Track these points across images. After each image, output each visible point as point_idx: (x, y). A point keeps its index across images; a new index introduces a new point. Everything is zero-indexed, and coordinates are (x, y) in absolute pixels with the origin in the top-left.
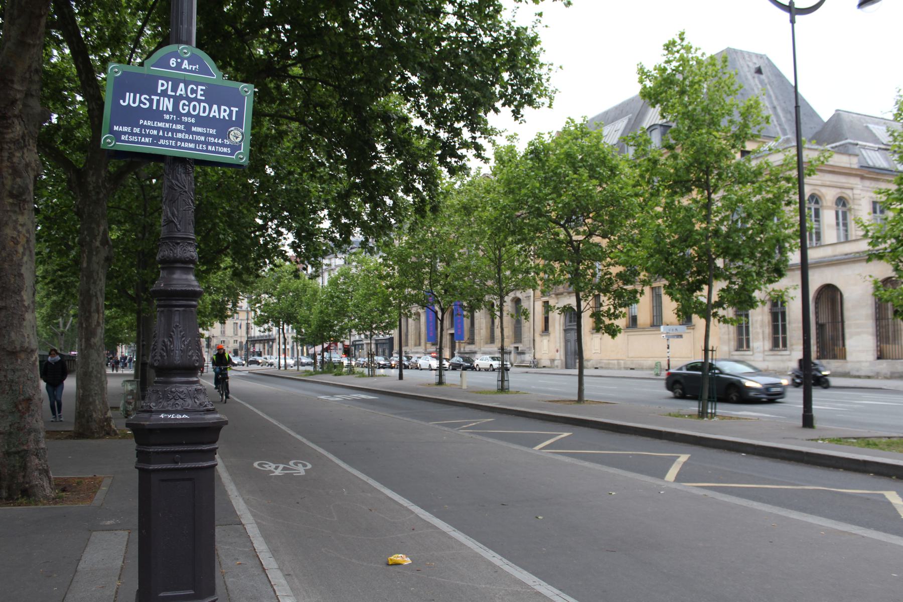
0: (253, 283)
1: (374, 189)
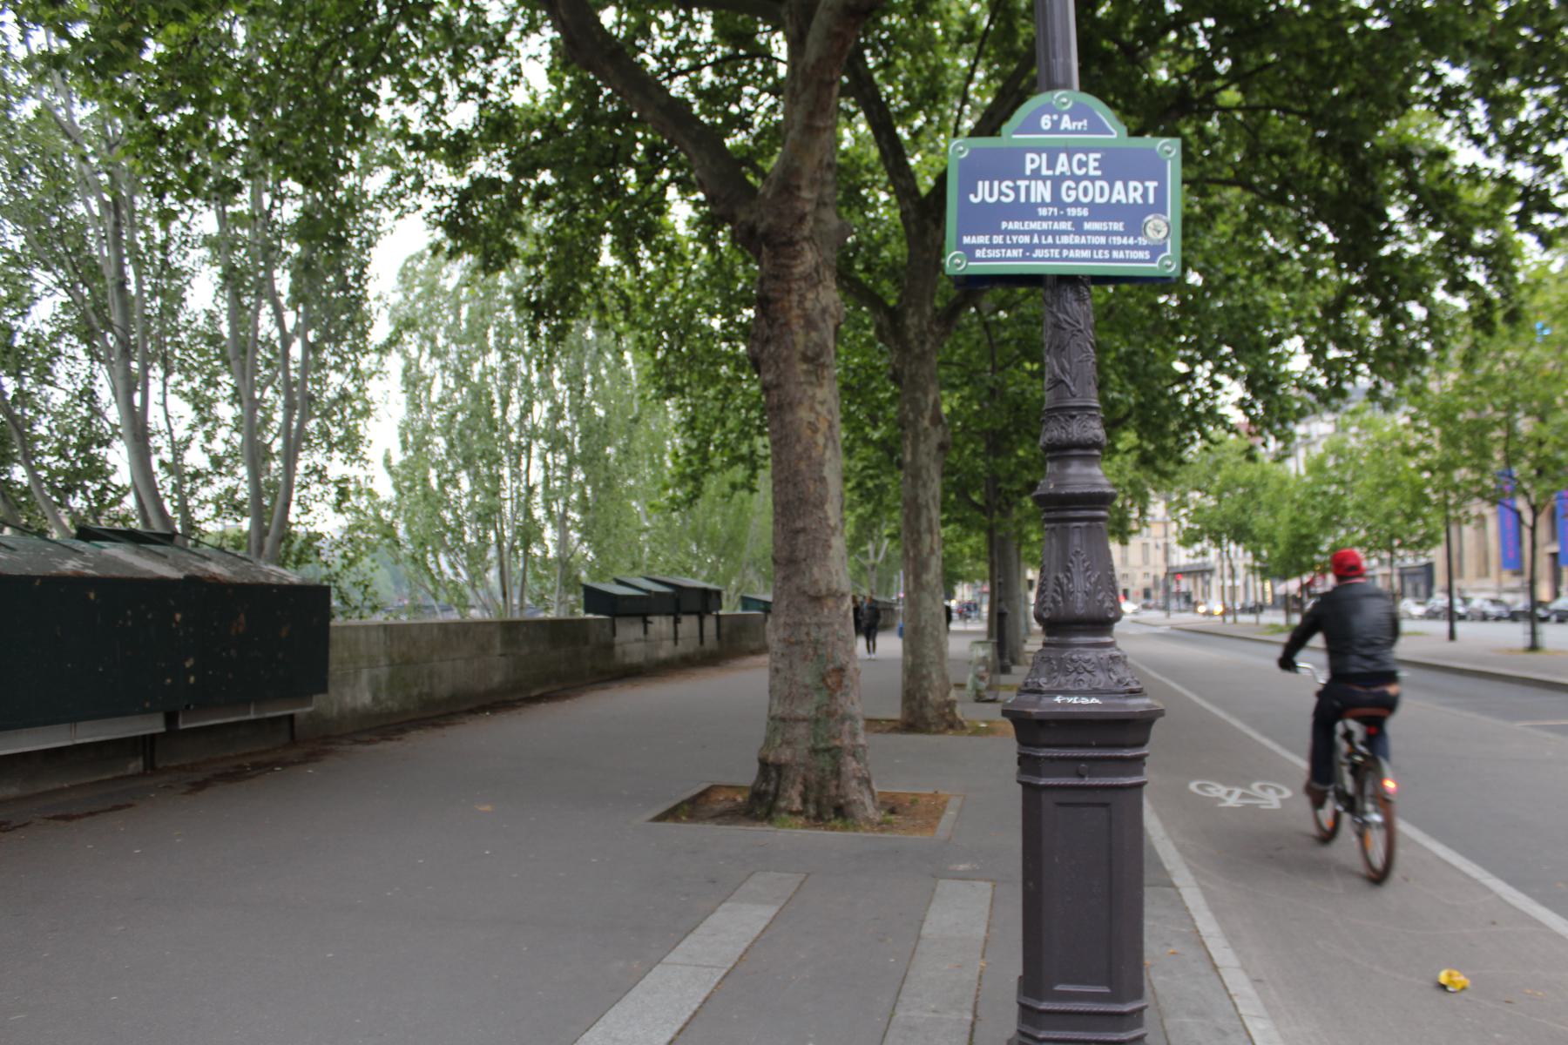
0: (1174, 473)
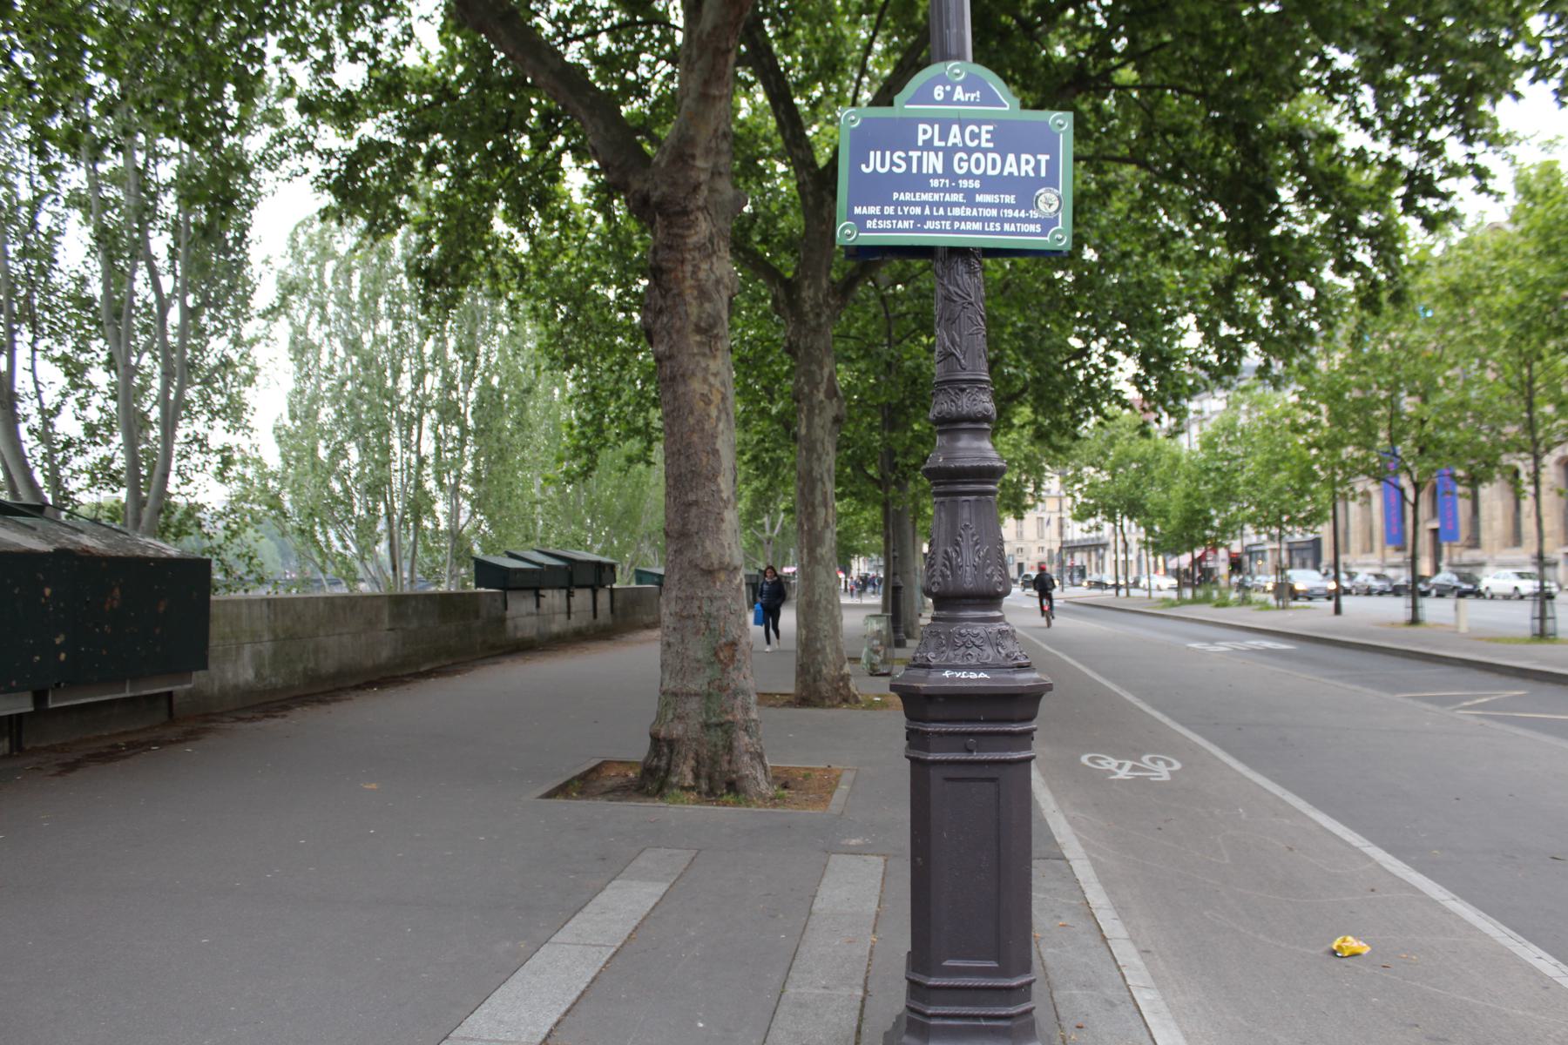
0: (1069, 448)
1: (1281, 272)
